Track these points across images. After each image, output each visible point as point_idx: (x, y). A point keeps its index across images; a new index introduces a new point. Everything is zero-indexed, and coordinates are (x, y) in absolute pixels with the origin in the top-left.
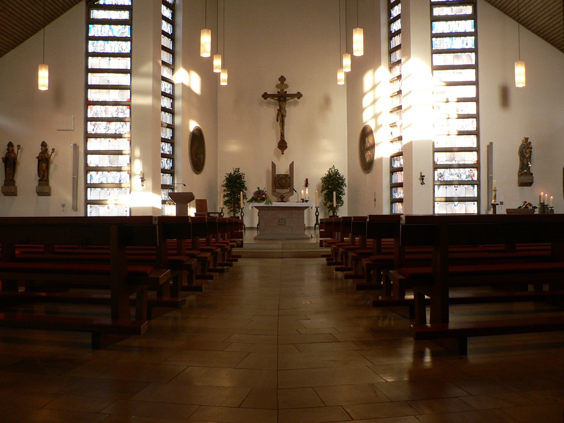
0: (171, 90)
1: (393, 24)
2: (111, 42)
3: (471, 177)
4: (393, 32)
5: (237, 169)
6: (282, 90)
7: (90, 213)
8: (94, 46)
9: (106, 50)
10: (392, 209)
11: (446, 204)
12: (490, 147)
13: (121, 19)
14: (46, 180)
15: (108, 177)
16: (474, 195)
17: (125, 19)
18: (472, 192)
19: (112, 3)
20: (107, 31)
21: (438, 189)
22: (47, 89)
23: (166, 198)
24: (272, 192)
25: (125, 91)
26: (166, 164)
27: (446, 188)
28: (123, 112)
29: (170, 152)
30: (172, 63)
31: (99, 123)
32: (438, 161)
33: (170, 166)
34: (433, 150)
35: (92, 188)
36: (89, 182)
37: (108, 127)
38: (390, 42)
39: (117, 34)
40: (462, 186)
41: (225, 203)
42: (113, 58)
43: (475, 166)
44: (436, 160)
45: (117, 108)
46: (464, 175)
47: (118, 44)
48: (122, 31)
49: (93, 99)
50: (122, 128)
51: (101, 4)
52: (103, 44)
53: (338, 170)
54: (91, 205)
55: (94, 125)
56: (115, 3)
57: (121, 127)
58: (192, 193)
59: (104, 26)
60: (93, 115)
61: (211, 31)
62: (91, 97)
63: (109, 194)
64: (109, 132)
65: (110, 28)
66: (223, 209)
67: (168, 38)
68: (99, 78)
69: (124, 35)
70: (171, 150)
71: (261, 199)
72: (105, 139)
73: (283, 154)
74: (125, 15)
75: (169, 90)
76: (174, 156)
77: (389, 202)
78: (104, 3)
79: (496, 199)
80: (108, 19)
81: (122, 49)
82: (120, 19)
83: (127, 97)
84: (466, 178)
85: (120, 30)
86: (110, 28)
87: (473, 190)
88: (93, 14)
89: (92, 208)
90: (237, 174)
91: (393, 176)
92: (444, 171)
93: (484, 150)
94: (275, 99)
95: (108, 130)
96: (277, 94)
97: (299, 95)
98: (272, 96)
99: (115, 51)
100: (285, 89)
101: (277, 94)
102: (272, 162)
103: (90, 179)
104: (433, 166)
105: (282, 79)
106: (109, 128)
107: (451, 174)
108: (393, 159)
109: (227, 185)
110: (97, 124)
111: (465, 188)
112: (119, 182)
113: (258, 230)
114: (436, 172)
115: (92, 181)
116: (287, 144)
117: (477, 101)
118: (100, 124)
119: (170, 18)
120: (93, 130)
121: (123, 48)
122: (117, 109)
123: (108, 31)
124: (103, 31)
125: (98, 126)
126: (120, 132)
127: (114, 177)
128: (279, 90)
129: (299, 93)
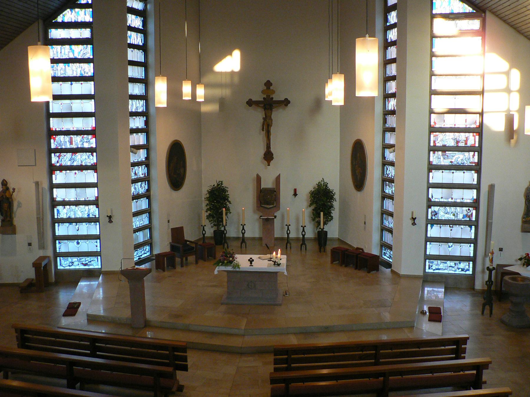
0: (145, 107)
1: (389, 31)
2: (72, 64)
3: (469, 217)
4: (389, 41)
5: (220, 182)
6: (268, 96)
7: (59, 248)
8: (54, 70)
9: (67, 74)
10: (383, 236)
11: (440, 245)
12: (492, 188)
13: (82, 38)
14: (9, 221)
16: (471, 237)
17: (87, 38)
18: (469, 233)
19: (71, 20)
20: (67, 53)
21: (431, 228)
23: (141, 224)
24: (257, 207)
25: (90, 118)
26: (140, 189)
27: (440, 227)
28: (88, 142)
29: (145, 173)
30: (144, 76)
31: (63, 154)
32: (432, 198)
33: (145, 189)
34: (427, 186)
35: (60, 223)
36: (56, 217)
37: (73, 158)
38: (386, 51)
39: (78, 56)
40: (457, 226)
41: (208, 217)
42: (75, 82)
43: (474, 205)
44: (430, 196)
45: (81, 138)
46: (460, 214)
47: (79, 66)
48: (84, 52)
49: (55, 129)
50: (88, 159)
51: (59, 22)
52: (64, 67)
53: (327, 184)
54: (59, 241)
55: (58, 157)
56: (75, 20)
57: (87, 158)
59: (64, 46)
60: (57, 146)
62: (53, 126)
63: (77, 229)
64: (75, 164)
65: (71, 49)
67: (138, 50)
68: (61, 105)
69: (86, 56)
70: (146, 172)
71: (227, 263)
72: (71, 171)
73: (269, 165)
74: (86, 33)
75: (142, 108)
76: (149, 178)
77: (380, 229)
78: (62, 20)
79: (492, 263)
80: (68, 38)
81: (85, 72)
82: (81, 38)
83: (92, 125)
84: (463, 218)
85: (81, 50)
86: (71, 49)
87: (470, 231)
88: (51, 33)
89: (61, 243)
90: (220, 187)
91: (384, 201)
92: (439, 209)
93: (484, 189)
95: (73, 162)
97: (286, 102)
98: (257, 103)
99: (77, 75)
102: (258, 175)
103: (57, 214)
104: (427, 203)
105: (268, 84)
107: (446, 213)
108: (385, 183)
109: (208, 199)
110: (61, 156)
111: (462, 228)
112: (87, 216)
114: (430, 210)
115: (60, 216)
116: (273, 155)
117: (480, 151)
118: (65, 156)
119: (141, 27)
120: (58, 162)
121: (85, 70)
122: (82, 138)
123: (69, 52)
124: (63, 52)
125: (62, 157)
126: (86, 164)
127: (82, 211)
128: (265, 96)
129: (286, 99)
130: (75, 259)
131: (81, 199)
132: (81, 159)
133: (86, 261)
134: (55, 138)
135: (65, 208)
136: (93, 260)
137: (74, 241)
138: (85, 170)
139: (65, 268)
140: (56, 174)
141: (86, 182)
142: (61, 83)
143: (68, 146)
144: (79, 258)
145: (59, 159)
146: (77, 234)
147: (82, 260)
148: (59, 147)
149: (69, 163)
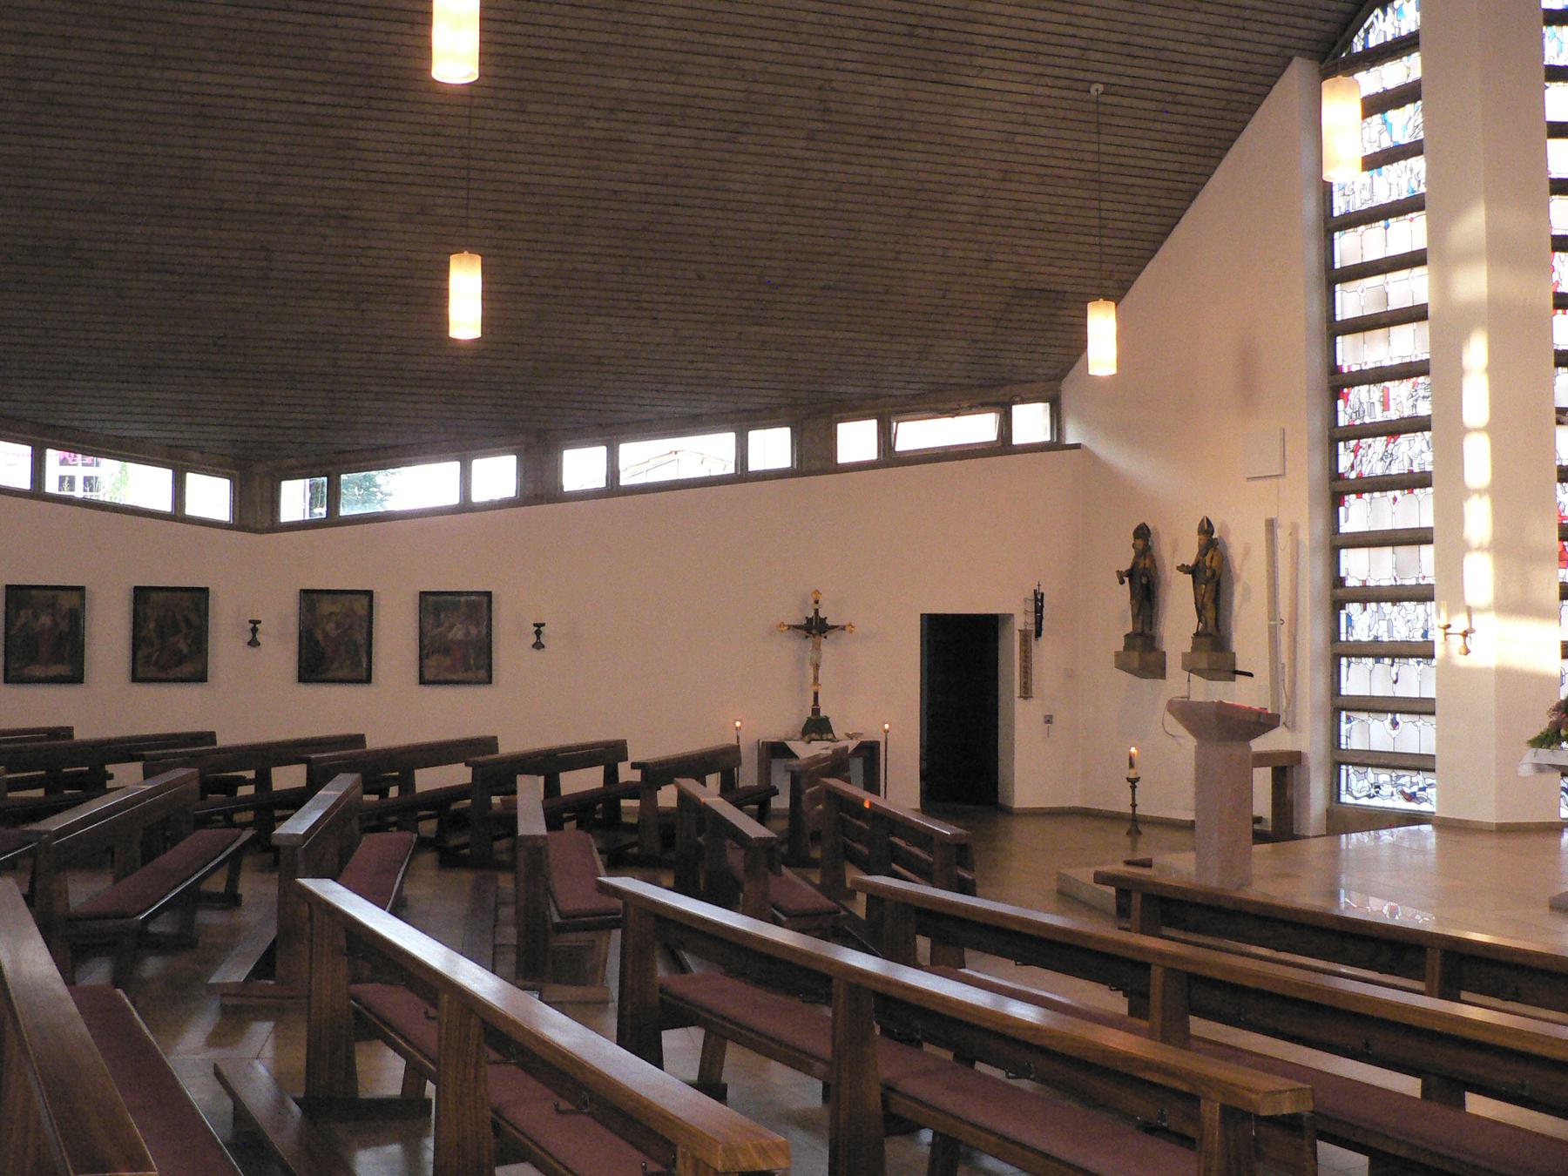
19: (1385, 37)
20: (1375, 137)
36: (1343, 638)
42: (1395, 219)
49: (1349, 367)
54: (1350, 714)
64: (1394, 470)
68: (1363, 295)
72: (1384, 494)
80: (1377, 93)
106: (1392, 454)
118: (1370, 446)
120: (1352, 467)
123: (1380, 133)
127: (1408, 621)
130: (1384, 777)
131: (1407, 582)
132: (1410, 453)
133: (1412, 784)
134: (1348, 394)
135: (1365, 609)
136: (1430, 785)
137: (1382, 716)
138: (1421, 487)
139: (1359, 802)
140: (1347, 504)
141: (1422, 526)
142: (1362, 228)
143: (1379, 416)
144: (1394, 775)
145: (1356, 456)
146: (1392, 695)
147: (1402, 781)
148: (1358, 422)
149: (1379, 470)
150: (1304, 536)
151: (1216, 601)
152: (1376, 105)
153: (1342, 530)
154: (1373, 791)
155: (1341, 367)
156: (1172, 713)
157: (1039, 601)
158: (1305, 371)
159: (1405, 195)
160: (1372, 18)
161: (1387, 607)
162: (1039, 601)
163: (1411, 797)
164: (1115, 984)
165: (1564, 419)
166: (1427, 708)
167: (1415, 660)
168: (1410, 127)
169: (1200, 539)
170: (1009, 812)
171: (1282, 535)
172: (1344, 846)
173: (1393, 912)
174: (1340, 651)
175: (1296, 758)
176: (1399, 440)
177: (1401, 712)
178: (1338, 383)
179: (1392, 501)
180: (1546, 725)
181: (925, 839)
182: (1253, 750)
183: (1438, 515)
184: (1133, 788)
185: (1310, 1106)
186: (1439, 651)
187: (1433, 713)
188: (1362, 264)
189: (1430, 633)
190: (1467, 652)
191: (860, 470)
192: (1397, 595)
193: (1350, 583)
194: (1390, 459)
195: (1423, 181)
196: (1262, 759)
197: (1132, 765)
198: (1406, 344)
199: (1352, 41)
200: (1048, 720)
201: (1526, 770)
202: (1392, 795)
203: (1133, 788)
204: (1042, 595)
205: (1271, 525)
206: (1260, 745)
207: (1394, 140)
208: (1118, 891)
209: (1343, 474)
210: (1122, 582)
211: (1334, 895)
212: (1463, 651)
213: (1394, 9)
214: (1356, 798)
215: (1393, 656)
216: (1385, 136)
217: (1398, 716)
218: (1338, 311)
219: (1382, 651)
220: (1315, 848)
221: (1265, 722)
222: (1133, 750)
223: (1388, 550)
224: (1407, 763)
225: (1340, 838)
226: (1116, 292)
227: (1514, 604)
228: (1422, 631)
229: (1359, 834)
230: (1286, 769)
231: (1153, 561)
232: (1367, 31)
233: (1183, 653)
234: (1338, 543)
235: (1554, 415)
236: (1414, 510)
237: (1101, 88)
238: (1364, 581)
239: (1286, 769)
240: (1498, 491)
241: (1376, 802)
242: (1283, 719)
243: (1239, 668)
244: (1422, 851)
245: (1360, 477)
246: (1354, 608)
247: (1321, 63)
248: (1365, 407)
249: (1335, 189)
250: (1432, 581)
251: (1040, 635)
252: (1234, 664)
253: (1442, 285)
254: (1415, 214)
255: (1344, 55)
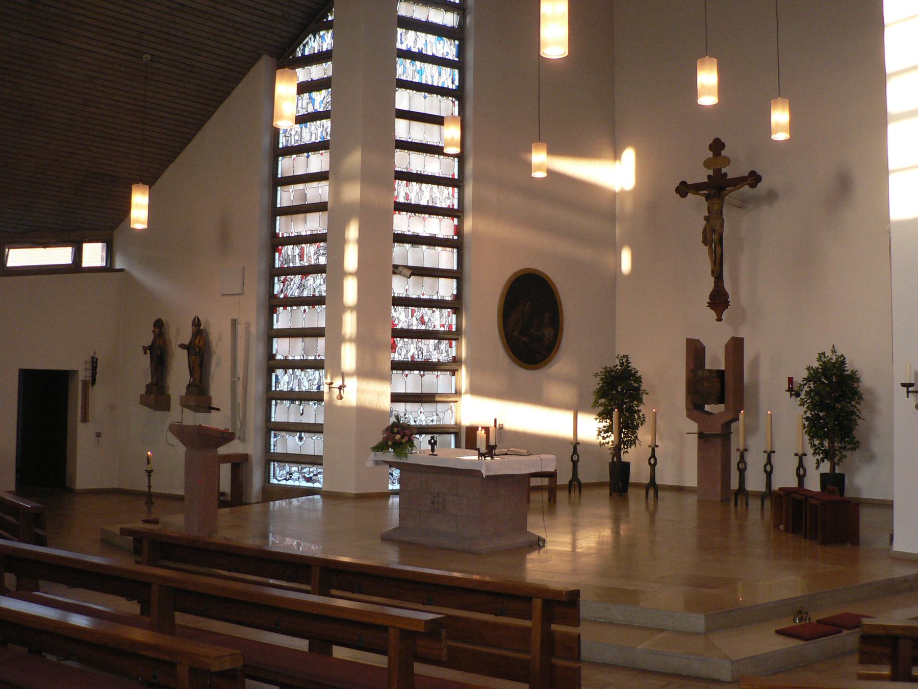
7: (274, 446)
15: (301, 379)
22: (147, 227)
23: (432, 421)
36: (273, 389)
42: (313, 153)
45: (316, 247)
58: (687, 416)
61: (718, 61)
64: (305, 294)
66: (772, 454)
67: (441, 96)
72: (299, 307)
85: (324, 97)
89: (277, 437)
94: (702, 195)
96: (707, 181)
98: (696, 188)
100: (722, 169)
101: (707, 181)
106: (304, 285)
113: (570, 493)
118: (292, 280)
123: (308, 104)
126: (320, 293)
127: (310, 380)
128: (711, 172)
133: (310, 472)
134: (281, 250)
135: (286, 373)
139: (280, 483)
141: (319, 326)
142: (294, 156)
147: (305, 470)
150: (253, 330)
151: (201, 365)
152: (305, 88)
153: (275, 327)
154: (288, 476)
155: (278, 233)
156: (173, 433)
157: (94, 362)
158: (260, 235)
159: (319, 140)
160: (307, 39)
161: (298, 372)
162: (94, 362)
163: (309, 480)
164: (130, 597)
165: (397, 271)
166: (319, 429)
167: (313, 402)
168: (324, 102)
169: (193, 329)
170: (72, 492)
171: (240, 329)
172: (271, 508)
173: (299, 545)
174: (272, 396)
175: (245, 458)
176: (309, 277)
177: (305, 432)
178: (276, 243)
179: (303, 311)
180: (381, 439)
181: (14, 509)
182: (219, 453)
183: (327, 321)
184: (149, 476)
185: (241, 663)
186: (326, 397)
187: (321, 432)
188: (294, 176)
189: (322, 387)
190: (341, 398)
191: (55, 273)
192: (304, 365)
193: (279, 357)
194: (302, 288)
195: (329, 133)
196: (225, 459)
197: (148, 462)
198: (314, 224)
199: (296, 50)
200: (98, 435)
201: (370, 464)
202: (299, 478)
203: (149, 476)
204: (97, 359)
205: (234, 322)
206: (223, 450)
207: (315, 108)
208: (135, 540)
209: (276, 295)
210: (145, 353)
211: (266, 537)
212: (339, 397)
213: (320, 36)
214: (279, 481)
215: (301, 400)
216: (310, 106)
217: (303, 434)
218: (278, 202)
219: (295, 397)
220: (256, 509)
221: (226, 437)
222: (149, 453)
223: (300, 340)
224: (308, 460)
225: (269, 504)
226: (150, 180)
227: (365, 372)
228: (317, 386)
229: (280, 501)
230: (239, 464)
231: (165, 341)
232: (304, 46)
233: (141, 395)
234: (273, 334)
235: (391, 269)
236: (316, 318)
237: (149, 57)
238: (286, 357)
239: (239, 464)
240: (359, 308)
241: (290, 483)
242: (237, 435)
243: (213, 406)
244: (315, 510)
245: (285, 297)
246: (279, 372)
247: (278, 60)
248: (291, 257)
249: (281, 132)
250: (324, 358)
251: (95, 384)
252: (210, 403)
253: (335, 192)
254: (324, 151)
255: (291, 57)
